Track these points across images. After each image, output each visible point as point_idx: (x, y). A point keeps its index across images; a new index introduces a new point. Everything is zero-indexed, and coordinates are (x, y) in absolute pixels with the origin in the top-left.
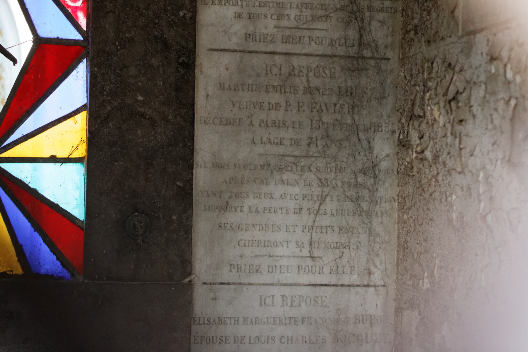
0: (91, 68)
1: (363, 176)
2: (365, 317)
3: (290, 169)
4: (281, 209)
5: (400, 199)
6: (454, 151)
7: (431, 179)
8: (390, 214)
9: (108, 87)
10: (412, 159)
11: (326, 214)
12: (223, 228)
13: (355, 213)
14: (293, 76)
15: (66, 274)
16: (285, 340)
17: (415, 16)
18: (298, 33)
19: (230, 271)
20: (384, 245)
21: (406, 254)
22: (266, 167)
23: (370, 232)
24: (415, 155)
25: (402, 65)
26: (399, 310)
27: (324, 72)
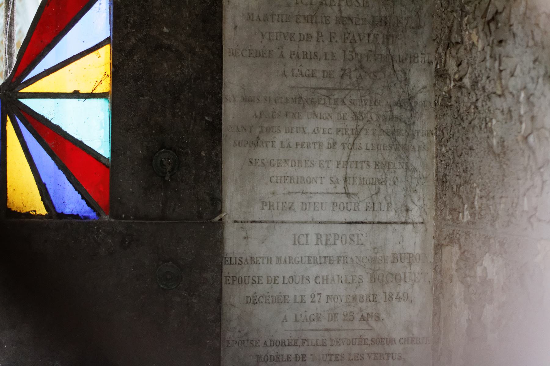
1: (399, 108)
2: (403, 255)
4: (314, 143)
5: (438, 132)
6: (494, 75)
7: (471, 106)
8: (428, 148)
10: (450, 89)
11: (361, 148)
12: (254, 164)
13: (391, 148)
15: (93, 215)
16: (320, 280)
19: (262, 209)
23: (407, 168)
26: (438, 247)
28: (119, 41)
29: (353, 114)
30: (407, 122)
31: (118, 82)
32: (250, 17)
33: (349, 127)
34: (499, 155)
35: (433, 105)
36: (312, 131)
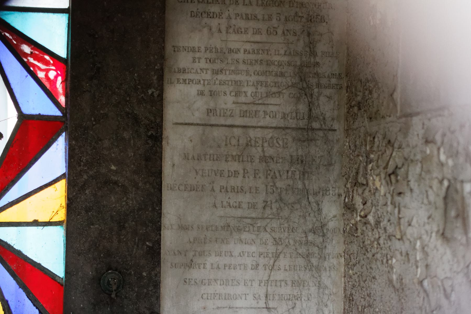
0: (69, 142)
1: (313, 234)
3: (247, 229)
4: (240, 265)
5: (346, 255)
7: (373, 242)
9: (85, 158)
10: (357, 222)
11: (280, 269)
12: (188, 284)
13: (306, 268)
14: (250, 147)
17: (358, 93)
18: (255, 108)
20: (332, 296)
21: (351, 305)
22: (226, 228)
23: (320, 286)
24: (359, 218)
25: (348, 135)
27: (277, 142)
28: (73, 178)
29: (273, 240)
30: (320, 246)
31: (71, 213)
32: (185, 156)
33: (270, 251)
34: (398, 290)
35: (342, 232)
36: (238, 255)
